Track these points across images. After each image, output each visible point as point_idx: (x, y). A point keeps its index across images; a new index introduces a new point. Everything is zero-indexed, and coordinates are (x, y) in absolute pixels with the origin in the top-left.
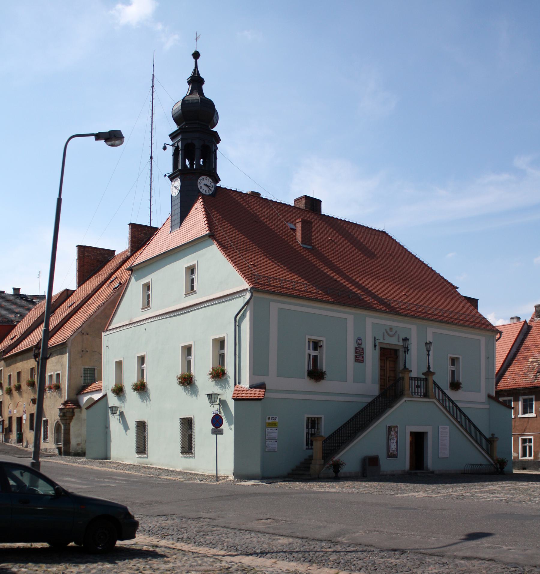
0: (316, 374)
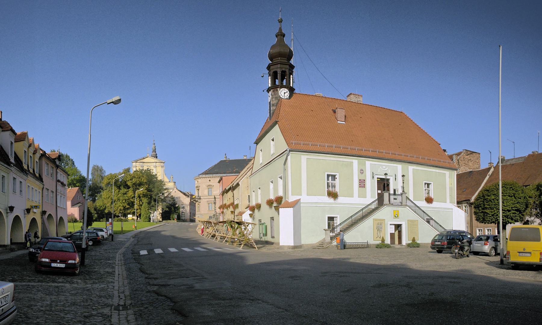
0: (333, 195)
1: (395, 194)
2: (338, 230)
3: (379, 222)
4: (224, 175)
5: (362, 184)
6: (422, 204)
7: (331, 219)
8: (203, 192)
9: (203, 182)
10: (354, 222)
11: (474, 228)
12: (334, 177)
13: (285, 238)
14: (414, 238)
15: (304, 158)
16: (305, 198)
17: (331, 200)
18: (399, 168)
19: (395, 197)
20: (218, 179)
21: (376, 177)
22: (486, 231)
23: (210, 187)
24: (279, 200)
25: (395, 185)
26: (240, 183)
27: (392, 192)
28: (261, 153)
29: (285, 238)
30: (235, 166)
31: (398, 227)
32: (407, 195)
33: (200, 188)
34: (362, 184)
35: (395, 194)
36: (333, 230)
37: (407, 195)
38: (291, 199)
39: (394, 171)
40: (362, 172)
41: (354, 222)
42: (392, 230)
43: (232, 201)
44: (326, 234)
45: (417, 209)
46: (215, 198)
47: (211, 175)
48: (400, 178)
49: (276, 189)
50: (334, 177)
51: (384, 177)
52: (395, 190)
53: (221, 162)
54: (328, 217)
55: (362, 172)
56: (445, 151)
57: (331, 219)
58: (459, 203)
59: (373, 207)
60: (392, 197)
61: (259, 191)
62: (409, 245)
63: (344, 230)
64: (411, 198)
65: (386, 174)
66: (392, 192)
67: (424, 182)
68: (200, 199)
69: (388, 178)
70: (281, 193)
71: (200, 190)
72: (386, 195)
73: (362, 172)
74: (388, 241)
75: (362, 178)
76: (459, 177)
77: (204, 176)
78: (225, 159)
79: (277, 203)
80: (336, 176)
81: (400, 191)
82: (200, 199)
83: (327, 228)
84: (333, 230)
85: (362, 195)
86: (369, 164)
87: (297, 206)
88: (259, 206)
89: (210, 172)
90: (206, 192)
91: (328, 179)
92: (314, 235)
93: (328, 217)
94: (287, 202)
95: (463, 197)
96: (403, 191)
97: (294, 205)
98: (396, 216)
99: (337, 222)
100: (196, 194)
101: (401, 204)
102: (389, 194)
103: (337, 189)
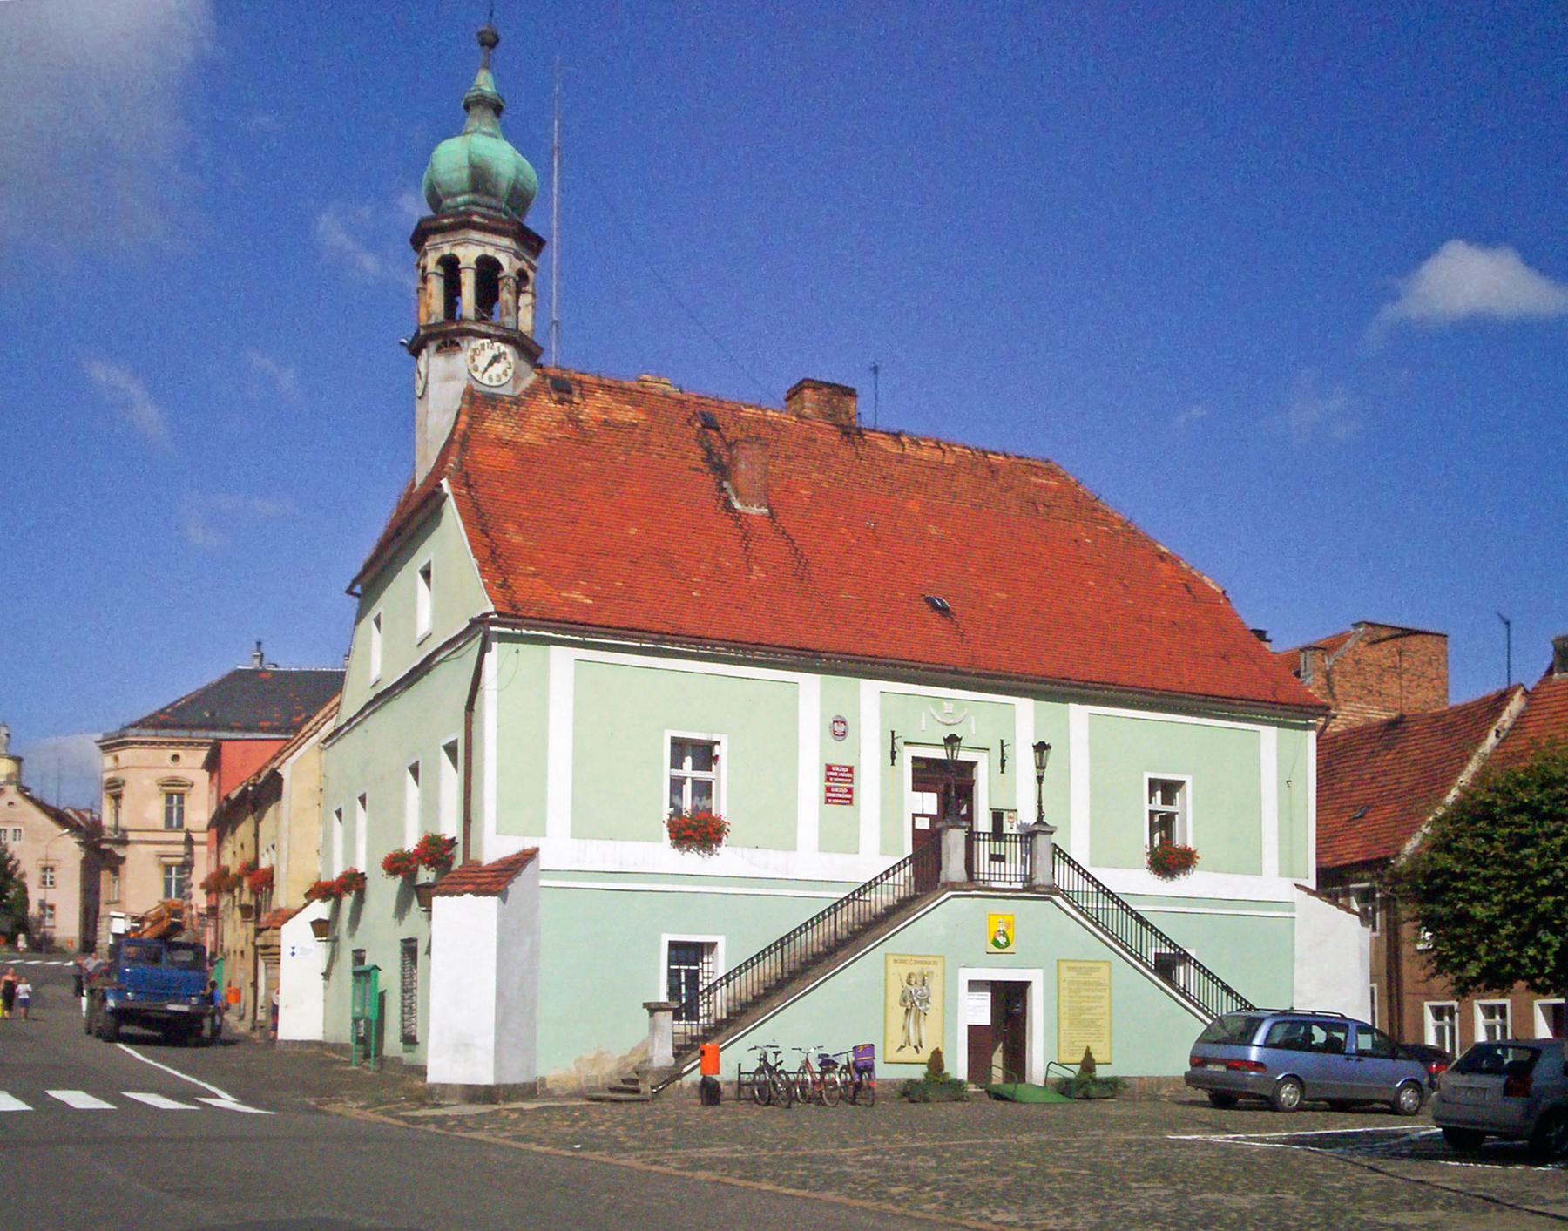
0: (697, 831)
1: (997, 834)
2: (718, 1005)
3: (915, 969)
4: (225, 735)
5: (839, 785)
6: (1135, 881)
7: (687, 954)
8: (142, 809)
9: (146, 769)
10: (802, 964)
11: (1408, 1001)
12: (704, 754)
13: (459, 1041)
14: (1088, 1054)
15: (562, 663)
16: (559, 851)
17: (692, 861)
18: (1025, 717)
19: (998, 848)
20: (203, 754)
21: (907, 755)
22: (1480, 1018)
23: (174, 793)
24: (436, 851)
25: (1003, 791)
26: (285, 772)
27: (984, 823)
28: (377, 639)
29: (459, 1041)
30: (291, 701)
31: (1010, 999)
32: (1055, 838)
33: (126, 791)
34: (839, 785)
35: (997, 834)
36: (686, 1011)
37: (1055, 838)
38: (493, 848)
39: (1000, 728)
40: (839, 729)
41: (802, 964)
42: (979, 1010)
43: (249, 855)
44: (654, 1028)
45: (1109, 915)
46: (189, 842)
47: (183, 735)
48: (1024, 759)
49: (430, 806)
50: (704, 754)
51: (940, 754)
52: (997, 817)
53: (238, 675)
54: (673, 945)
55: (839, 729)
56: (1261, 634)
57: (687, 954)
58: (1332, 882)
59: (883, 897)
60: (983, 849)
61: (362, 817)
62: (1065, 1088)
63: (744, 1013)
64: (1080, 854)
65: (952, 741)
66: (984, 823)
67: (1147, 775)
68: (124, 842)
69: (963, 756)
70: (450, 828)
71: (124, 802)
72: (954, 840)
73: (840, 728)
74: (958, 1066)
75: (840, 757)
76: (1332, 757)
77: (148, 734)
78: (256, 664)
79: (433, 869)
80: (717, 750)
81: (1029, 817)
82: (124, 842)
83: (663, 997)
84: (686, 1011)
85: (839, 842)
86: (871, 699)
87: (516, 887)
88: (354, 882)
89: (171, 722)
90: (155, 811)
91: (676, 763)
92: (604, 1027)
93: (673, 945)
94: (473, 867)
95: (1350, 853)
96: (1040, 821)
97: (497, 879)
98: (1000, 944)
99: (714, 967)
100: (107, 820)
101: (1030, 888)
102: (971, 838)
103: (721, 805)
